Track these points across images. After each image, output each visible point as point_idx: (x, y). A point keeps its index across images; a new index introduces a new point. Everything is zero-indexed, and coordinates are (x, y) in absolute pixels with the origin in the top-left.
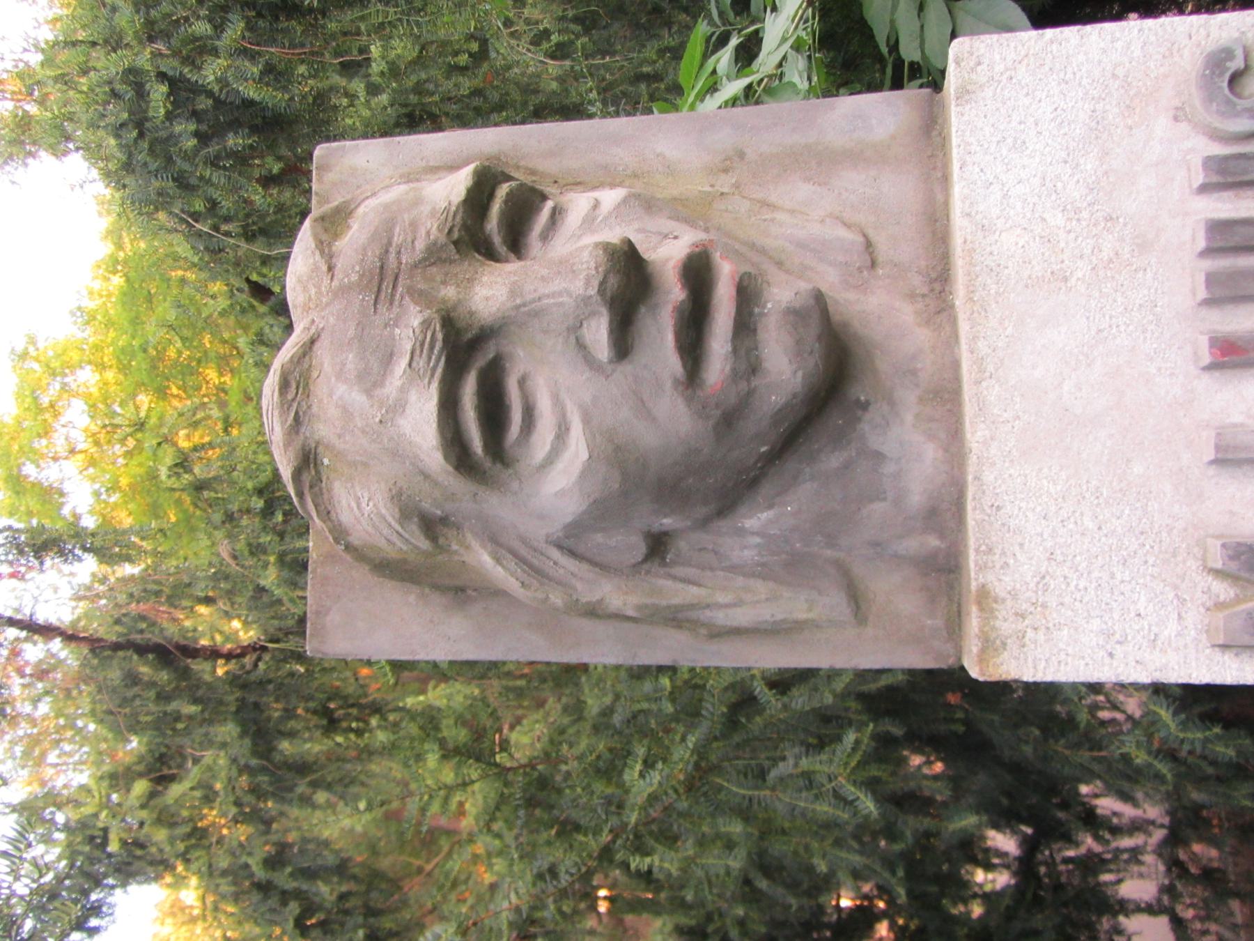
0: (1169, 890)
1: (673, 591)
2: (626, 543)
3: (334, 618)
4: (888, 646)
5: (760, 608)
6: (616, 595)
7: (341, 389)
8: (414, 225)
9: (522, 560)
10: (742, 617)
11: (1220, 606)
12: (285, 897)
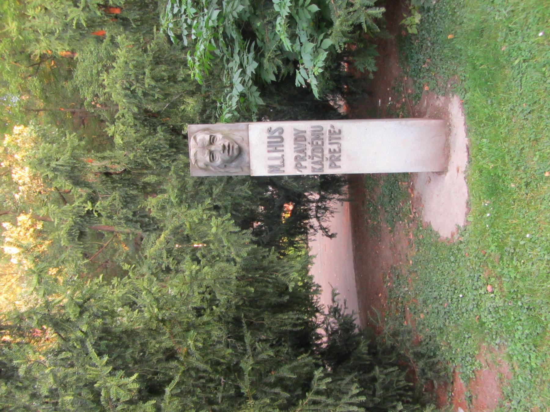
1: (227, 170)
4: (242, 173)
5: (234, 171)
6: (222, 170)
12: (136, 222)
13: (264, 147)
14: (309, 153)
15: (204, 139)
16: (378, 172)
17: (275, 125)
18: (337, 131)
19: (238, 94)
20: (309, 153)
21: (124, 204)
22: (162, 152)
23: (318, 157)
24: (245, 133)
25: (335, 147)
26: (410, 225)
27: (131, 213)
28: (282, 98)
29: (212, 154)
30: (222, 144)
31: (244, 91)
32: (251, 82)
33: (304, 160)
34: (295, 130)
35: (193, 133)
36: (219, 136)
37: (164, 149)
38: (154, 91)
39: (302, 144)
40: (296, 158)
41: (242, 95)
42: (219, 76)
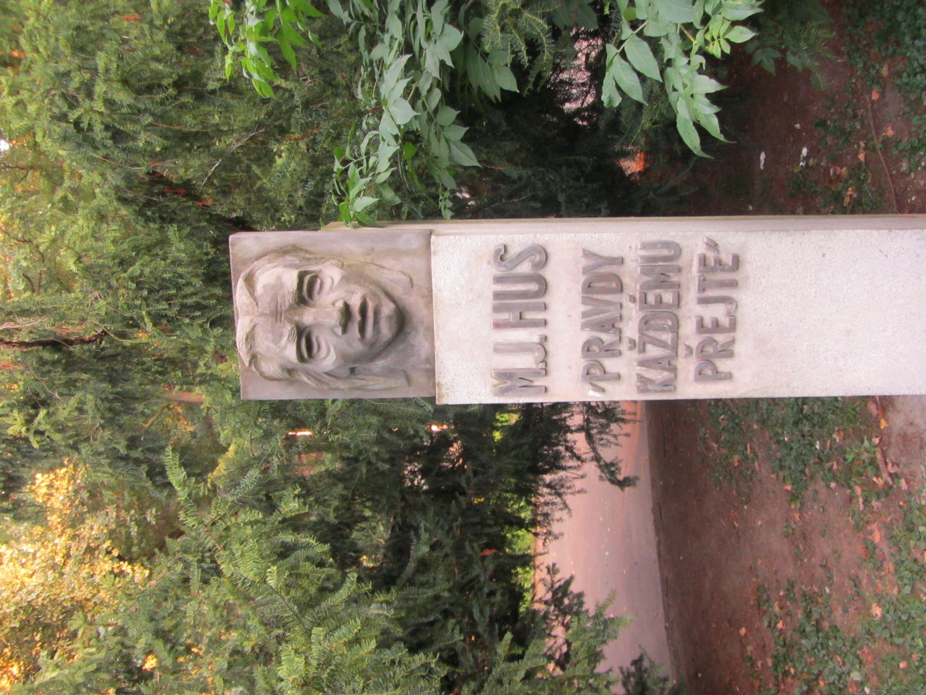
0: (587, 421)
1: (358, 383)
2: (345, 372)
3: (250, 388)
5: (379, 386)
6: (341, 385)
7: (267, 343)
8: (283, 296)
9: (316, 379)
10: (377, 387)
11: (495, 386)
12: (137, 462)
13: (481, 313)
14: (631, 330)
15: (278, 285)
16: (850, 394)
17: (519, 234)
18: (727, 260)
19: (396, 132)
20: (631, 330)
21: (108, 415)
22: (185, 297)
23: (662, 344)
24: (419, 263)
25: (718, 312)
26: (875, 503)
27: (124, 443)
28: (543, 150)
29: (305, 339)
30: (340, 304)
31: (416, 126)
32: (437, 94)
33: (613, 355)
34: (587, 254)
35: (245, 262)
36: (331, 274)
37: (189, 290)
38: (136, 122)
39: (609, 303)
40: (587, 348)
41: (409, 136)
42: (348, 87)
